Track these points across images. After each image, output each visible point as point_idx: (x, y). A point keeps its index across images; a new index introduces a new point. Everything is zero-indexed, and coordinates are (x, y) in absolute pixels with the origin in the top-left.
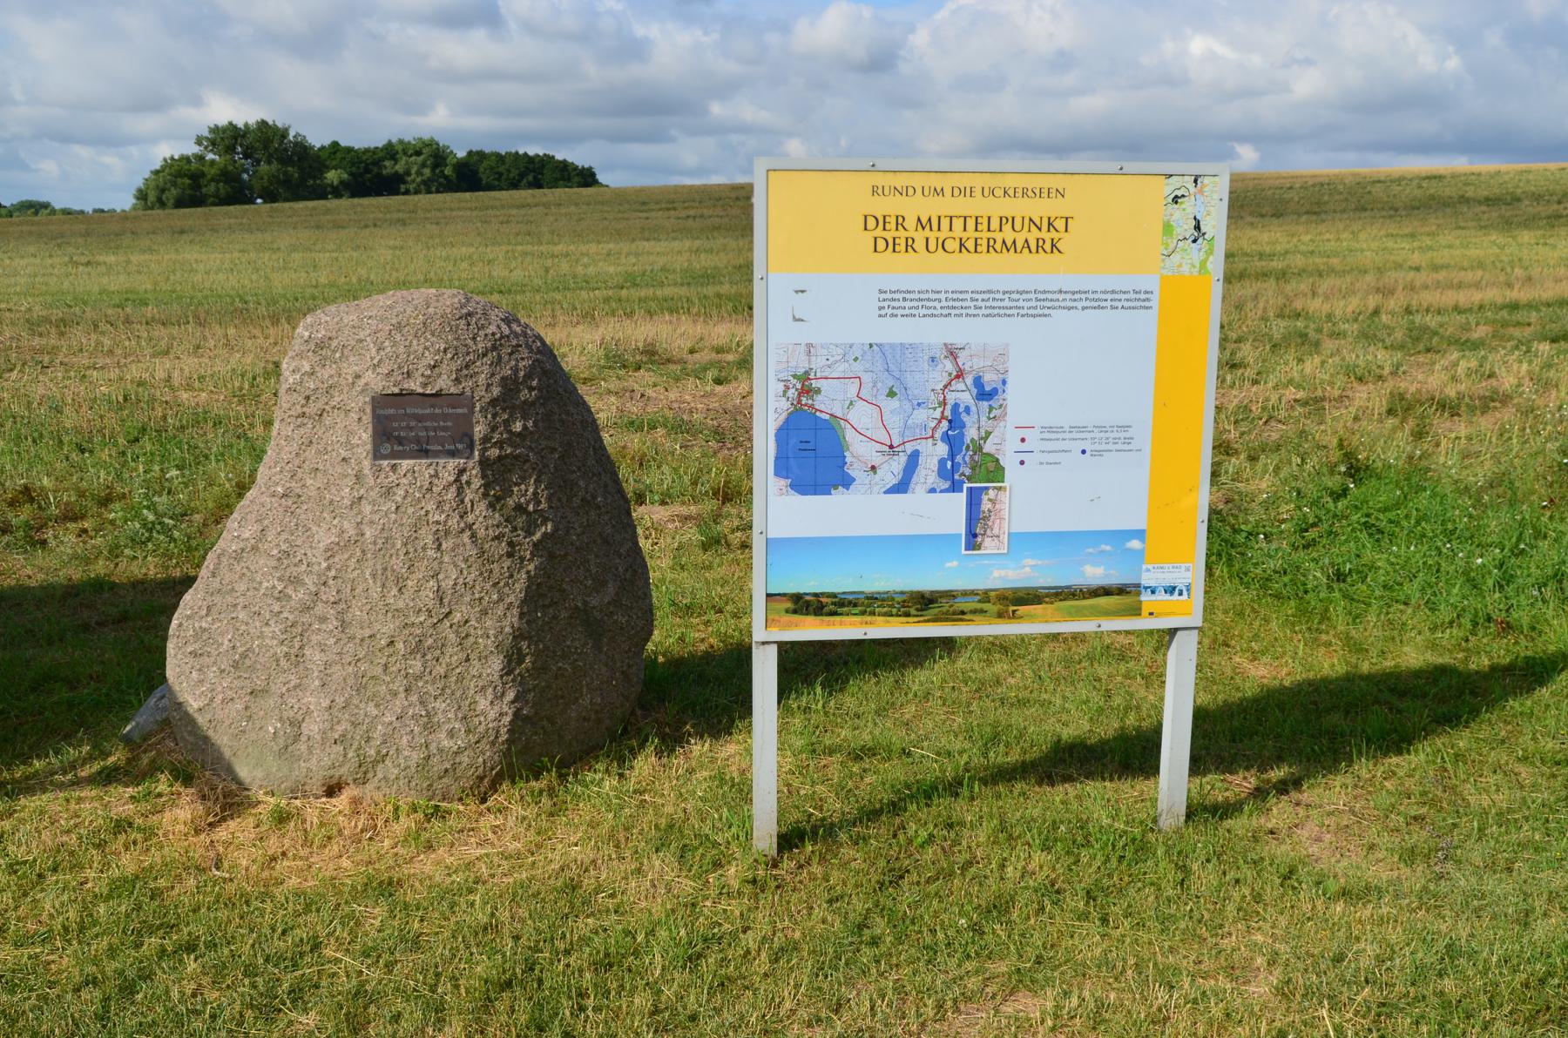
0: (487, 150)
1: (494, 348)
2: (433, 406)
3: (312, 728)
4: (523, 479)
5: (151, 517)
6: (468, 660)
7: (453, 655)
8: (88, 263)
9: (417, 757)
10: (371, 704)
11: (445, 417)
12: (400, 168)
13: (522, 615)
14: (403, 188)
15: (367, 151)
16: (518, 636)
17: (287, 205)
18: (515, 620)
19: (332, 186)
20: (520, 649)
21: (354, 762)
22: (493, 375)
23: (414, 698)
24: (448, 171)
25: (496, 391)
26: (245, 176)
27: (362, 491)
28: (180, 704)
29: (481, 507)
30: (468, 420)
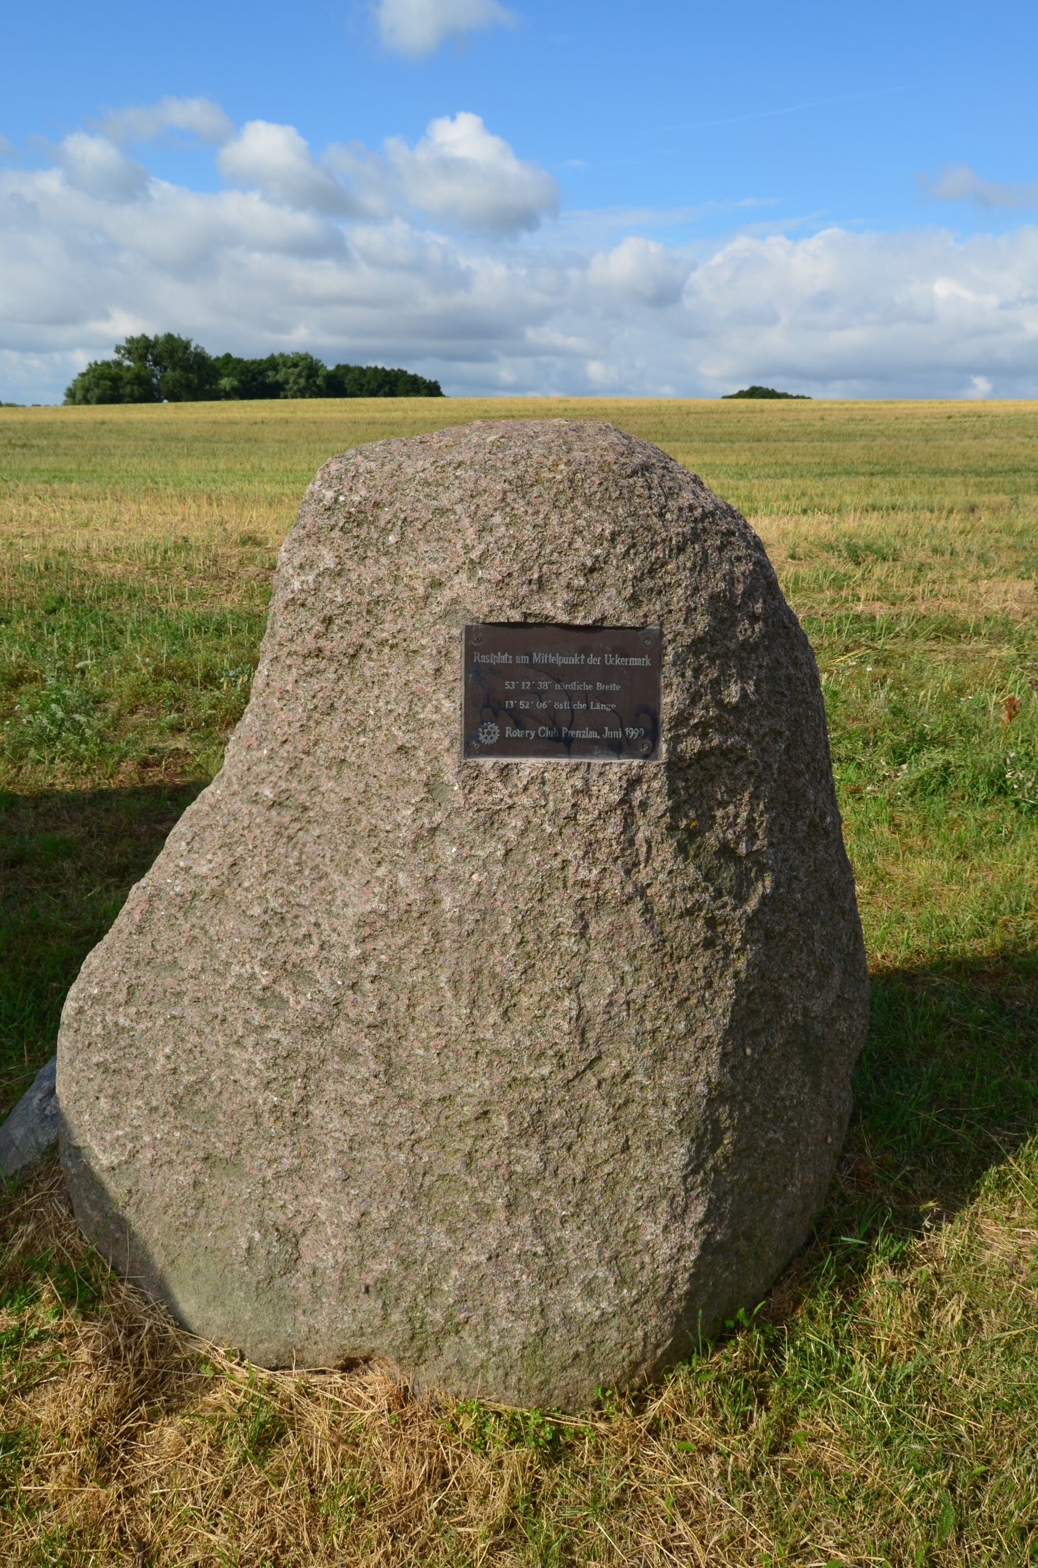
0: (352, 365)
1: (695, 537)
2: (585, 651)
3: (323, 1253)
4: (732, 792)
5: (60, 714)
6: (626, 1148)
7: (598, 1139)
8: (24, 446)
9: (522, 1331)
10: (439, 1228)
11: (607, 673)
12: (280, 377)
13: (724, 1056)
14: (282, 394)
15: (254, 362)
16: (718, 1096)
17: (189, 404)
18: (713, 1069)
19: (224, 390)
20: (716, 1122)
21: (403, 1331)
22: (696, 590)
23: (524, 1222)
24: (319, 381)
25: (702, 623)
26: (154, 380)
27: (438, 817)
28: (78, 1149)
29: (665, 853)
30: (649, 683)
